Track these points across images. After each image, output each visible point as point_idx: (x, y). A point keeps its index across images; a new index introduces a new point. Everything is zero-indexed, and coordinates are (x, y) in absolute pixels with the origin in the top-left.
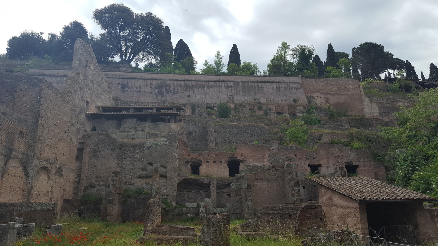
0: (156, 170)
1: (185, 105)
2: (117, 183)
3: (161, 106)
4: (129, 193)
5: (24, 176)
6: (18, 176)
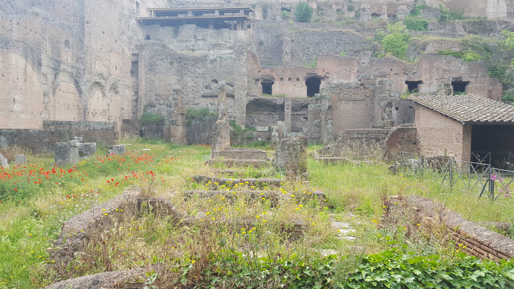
0: (222, 89)
1: (254, 6)
2: (179, 102)
3: (225, 7)
4: (193, 114)
5: (77, 92)
6: (71, 92)
